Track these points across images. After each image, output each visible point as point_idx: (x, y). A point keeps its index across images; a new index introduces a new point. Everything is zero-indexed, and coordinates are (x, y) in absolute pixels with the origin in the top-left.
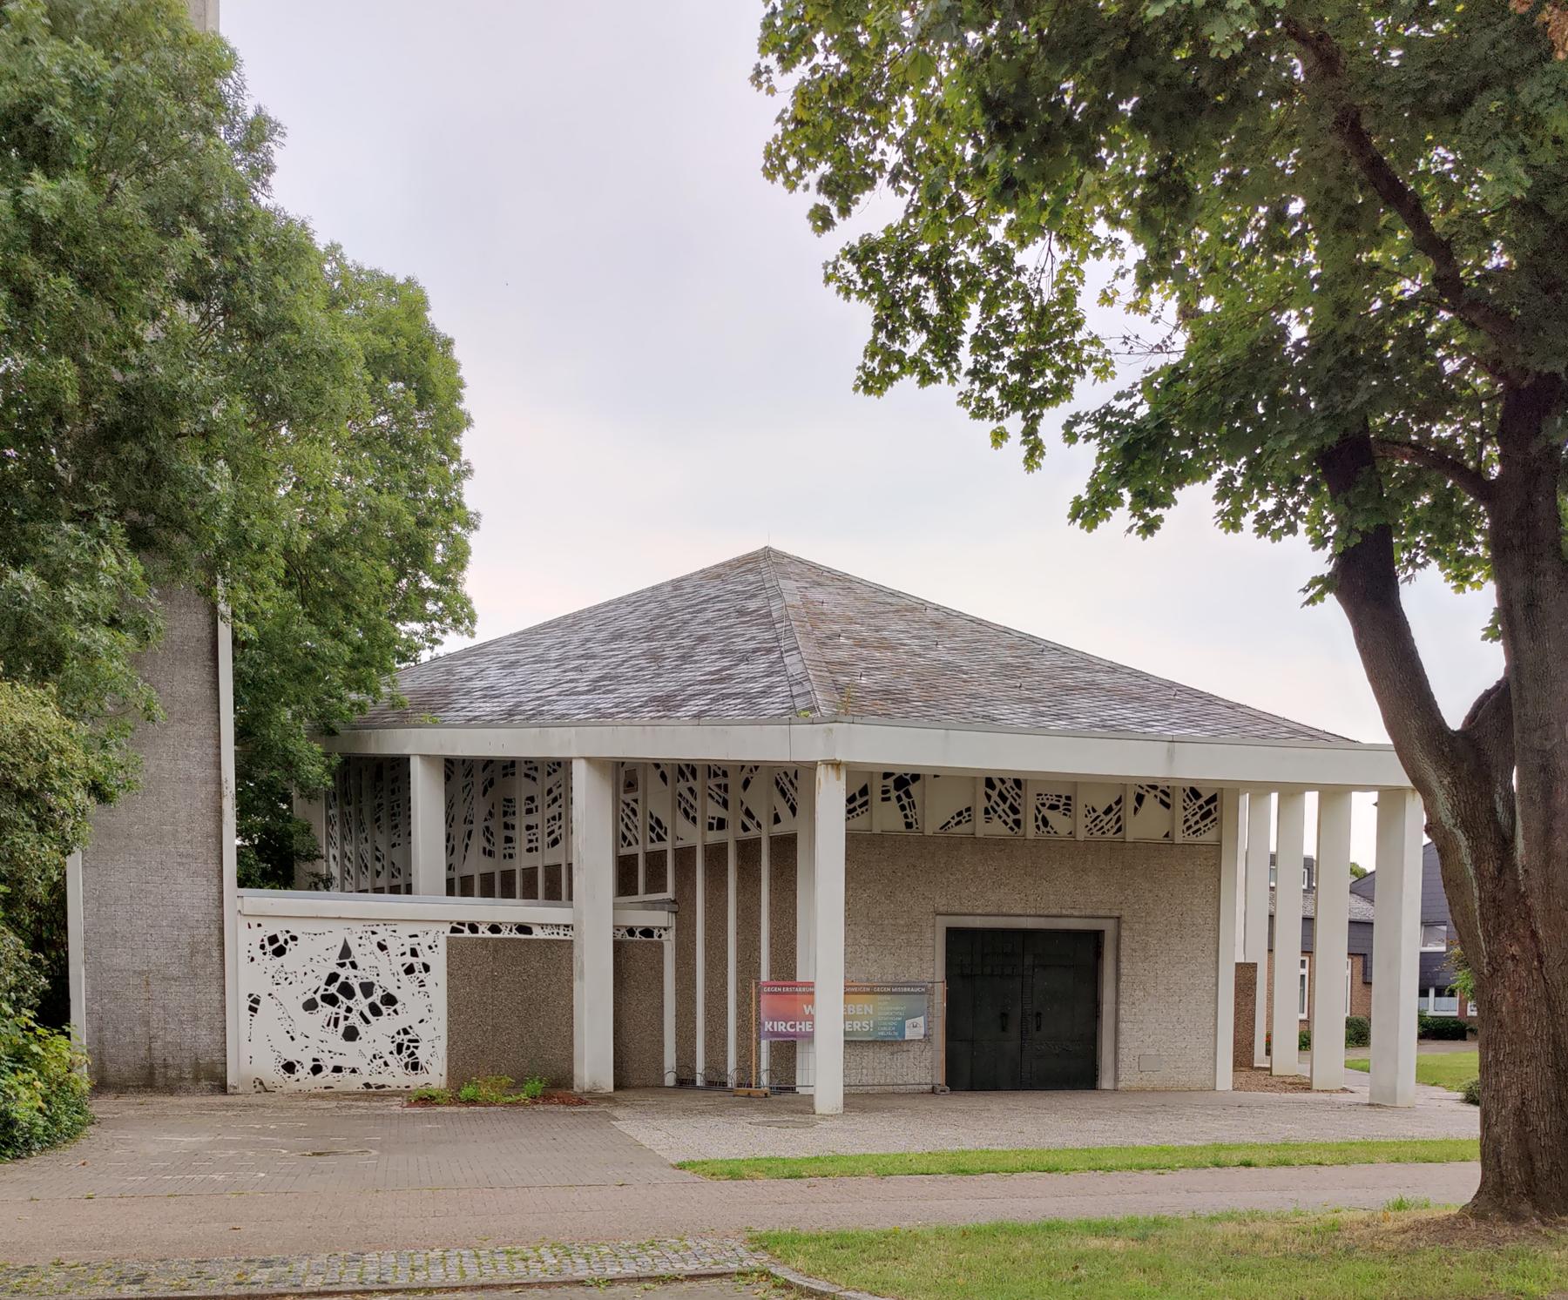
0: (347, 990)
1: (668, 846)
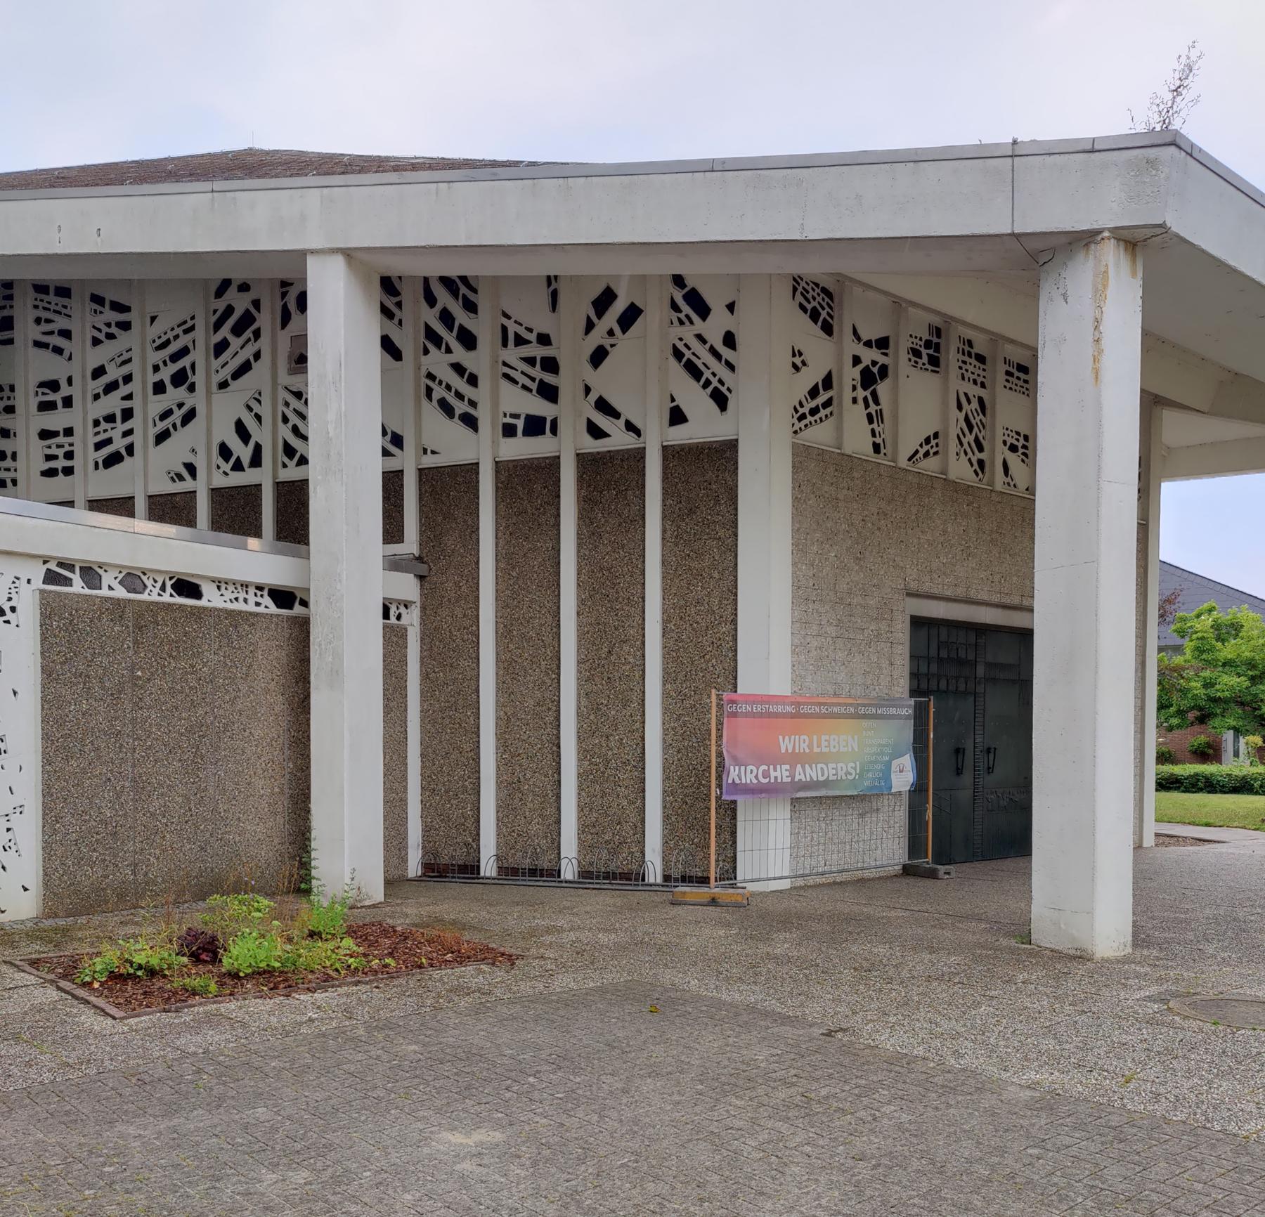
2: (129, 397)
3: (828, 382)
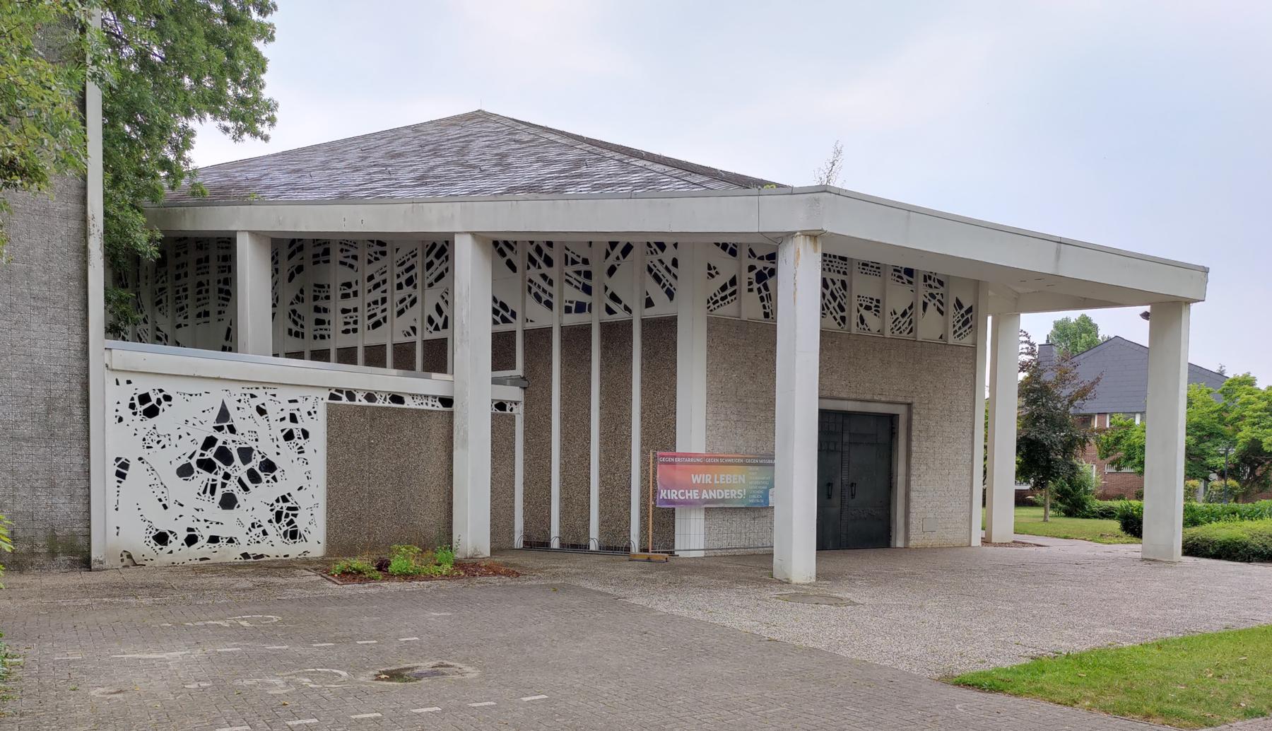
0: (224, 455)
1: (517, 326)
2: (385, 291)
3: (733, 282)
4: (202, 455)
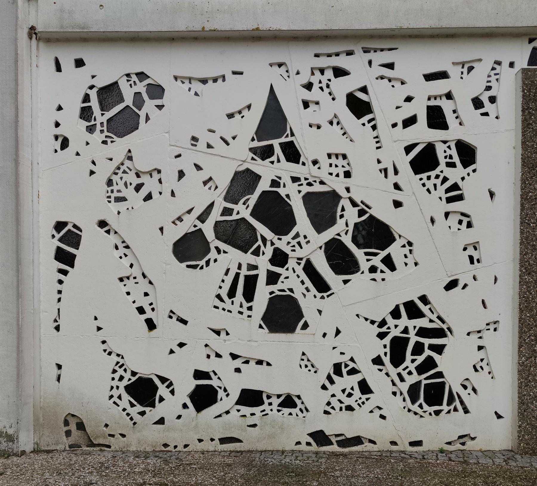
0: (275, 213)
4: (227, 212)
